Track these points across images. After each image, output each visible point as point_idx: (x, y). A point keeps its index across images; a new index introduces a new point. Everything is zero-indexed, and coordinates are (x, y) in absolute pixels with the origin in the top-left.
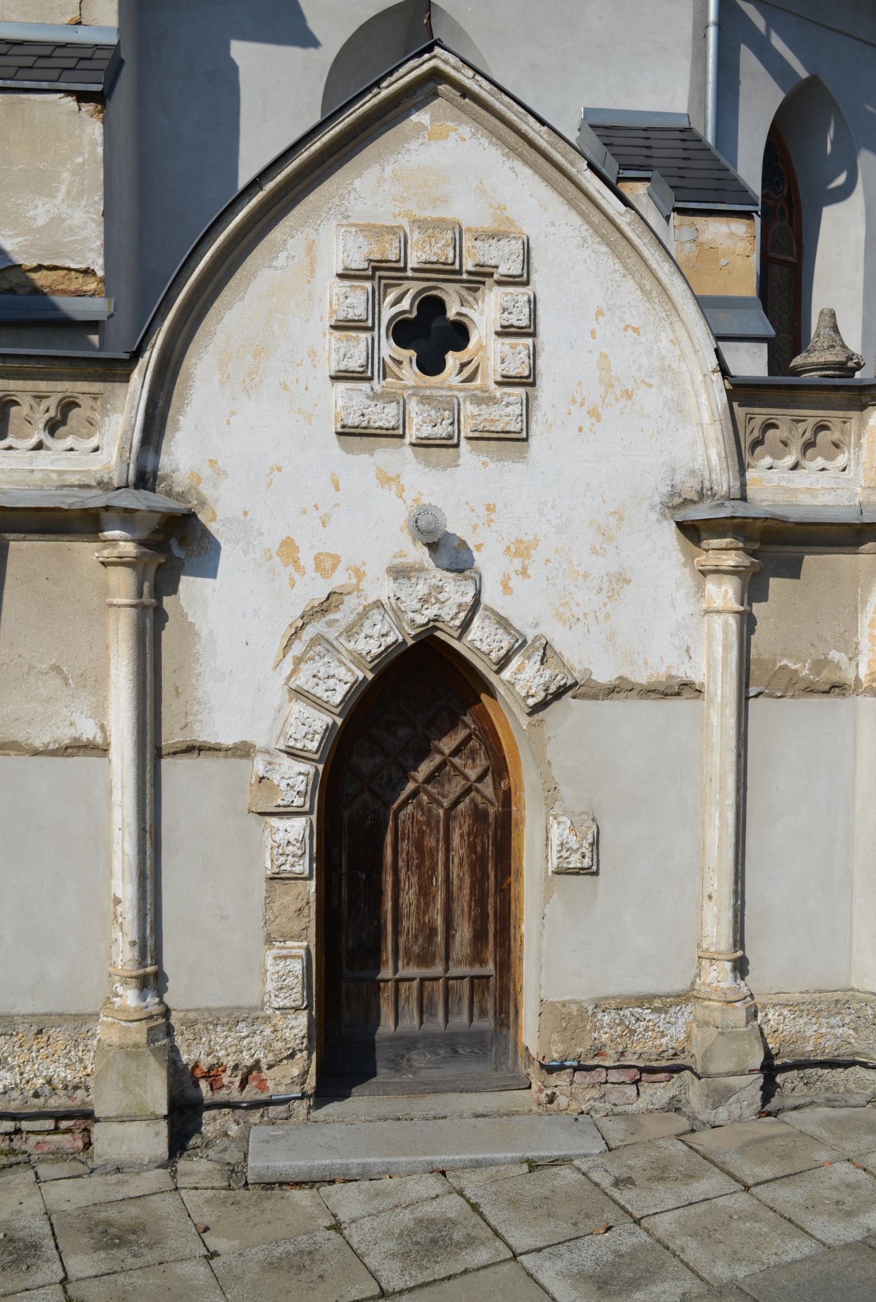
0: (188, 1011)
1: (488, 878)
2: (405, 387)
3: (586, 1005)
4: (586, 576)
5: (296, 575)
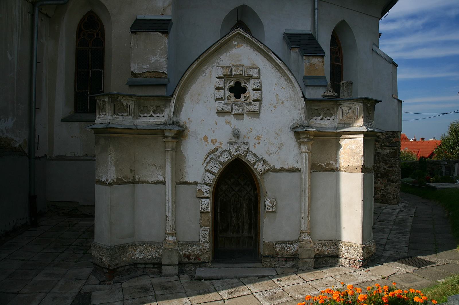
0: (183, 242)
2: (232, 102)
4: (273, 144)
5: (207, 144)
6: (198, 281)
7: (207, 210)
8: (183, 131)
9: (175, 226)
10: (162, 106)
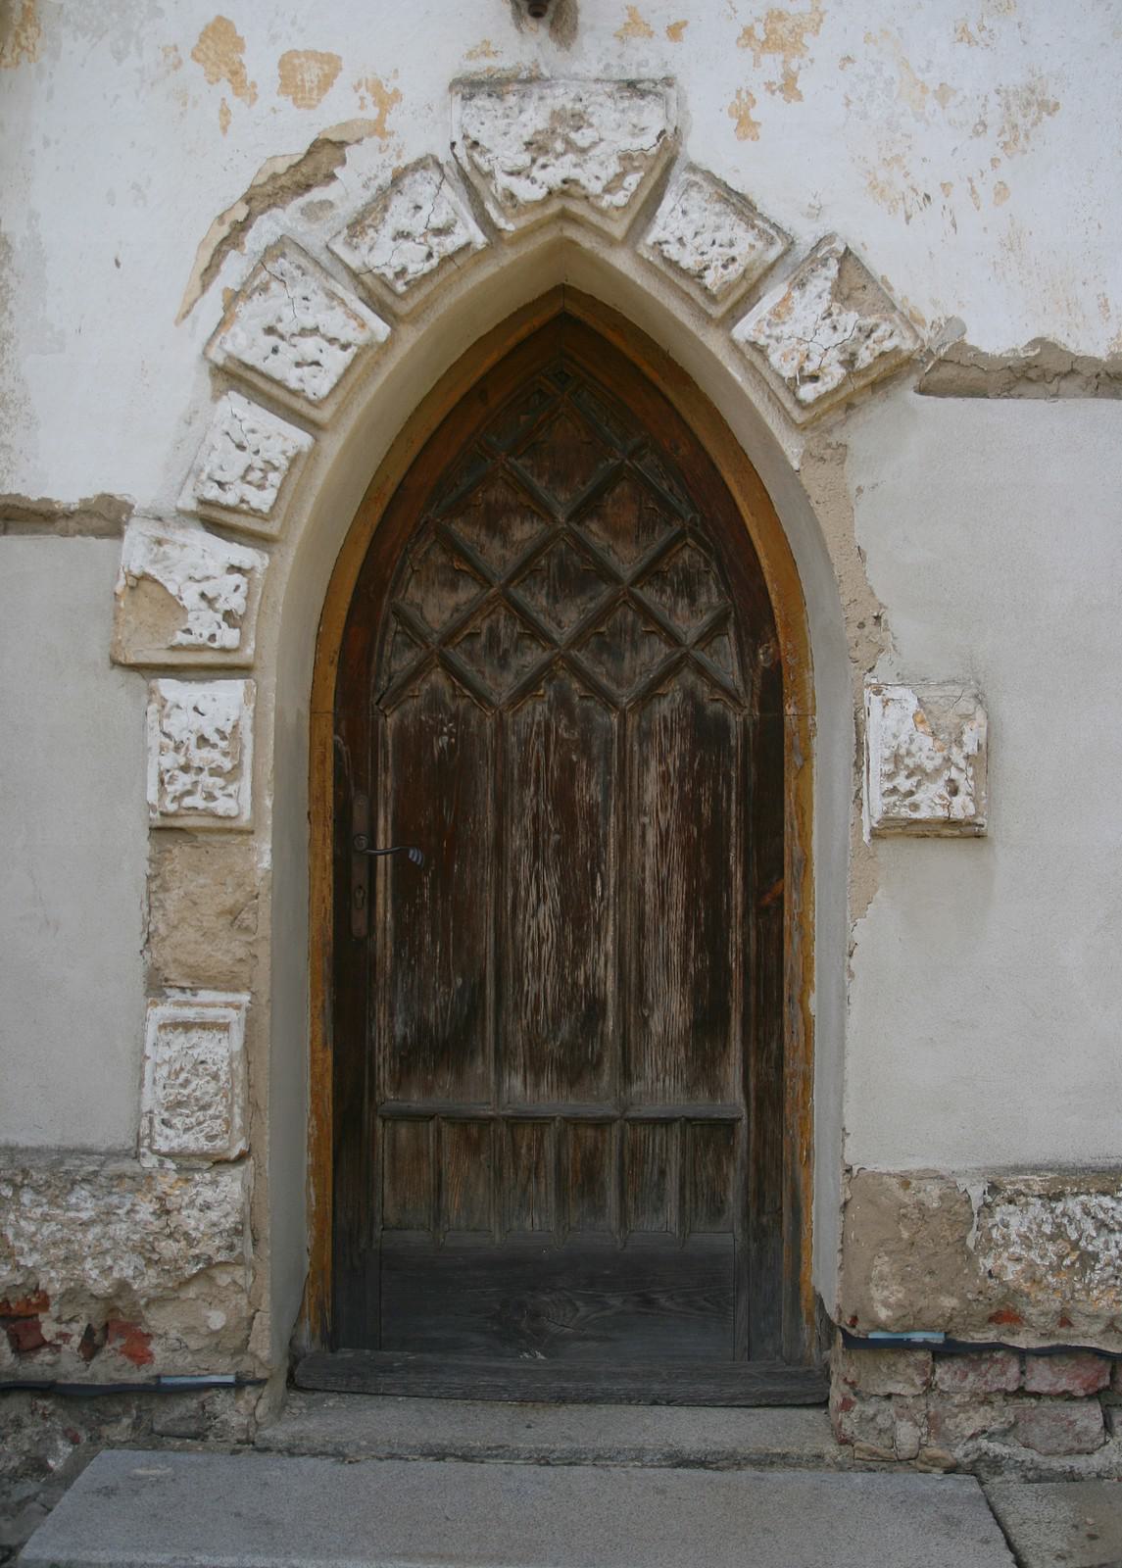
1: (729, 884)
3: (963, 1183)
4: (943, 93)
5: (235, 103)
7: (222, 806)
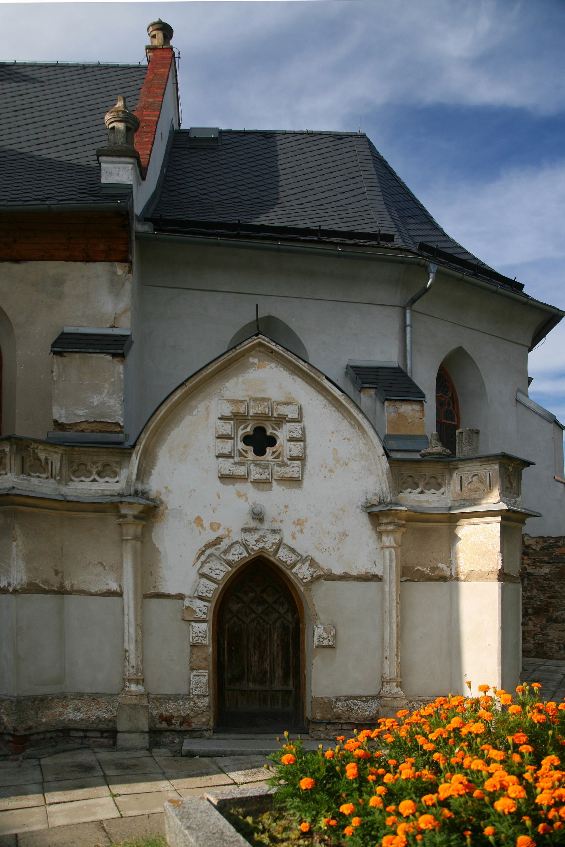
2: (248, 460)
4: (329, 533)
5: (202, 531)
6: (188, 758)
7: (204, 642)
8: (156, 507)
9: (141, 667)
10: (115, 465)
